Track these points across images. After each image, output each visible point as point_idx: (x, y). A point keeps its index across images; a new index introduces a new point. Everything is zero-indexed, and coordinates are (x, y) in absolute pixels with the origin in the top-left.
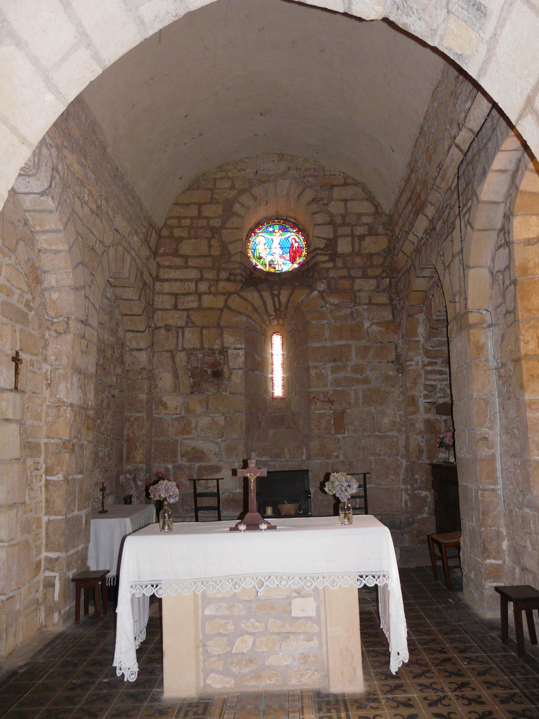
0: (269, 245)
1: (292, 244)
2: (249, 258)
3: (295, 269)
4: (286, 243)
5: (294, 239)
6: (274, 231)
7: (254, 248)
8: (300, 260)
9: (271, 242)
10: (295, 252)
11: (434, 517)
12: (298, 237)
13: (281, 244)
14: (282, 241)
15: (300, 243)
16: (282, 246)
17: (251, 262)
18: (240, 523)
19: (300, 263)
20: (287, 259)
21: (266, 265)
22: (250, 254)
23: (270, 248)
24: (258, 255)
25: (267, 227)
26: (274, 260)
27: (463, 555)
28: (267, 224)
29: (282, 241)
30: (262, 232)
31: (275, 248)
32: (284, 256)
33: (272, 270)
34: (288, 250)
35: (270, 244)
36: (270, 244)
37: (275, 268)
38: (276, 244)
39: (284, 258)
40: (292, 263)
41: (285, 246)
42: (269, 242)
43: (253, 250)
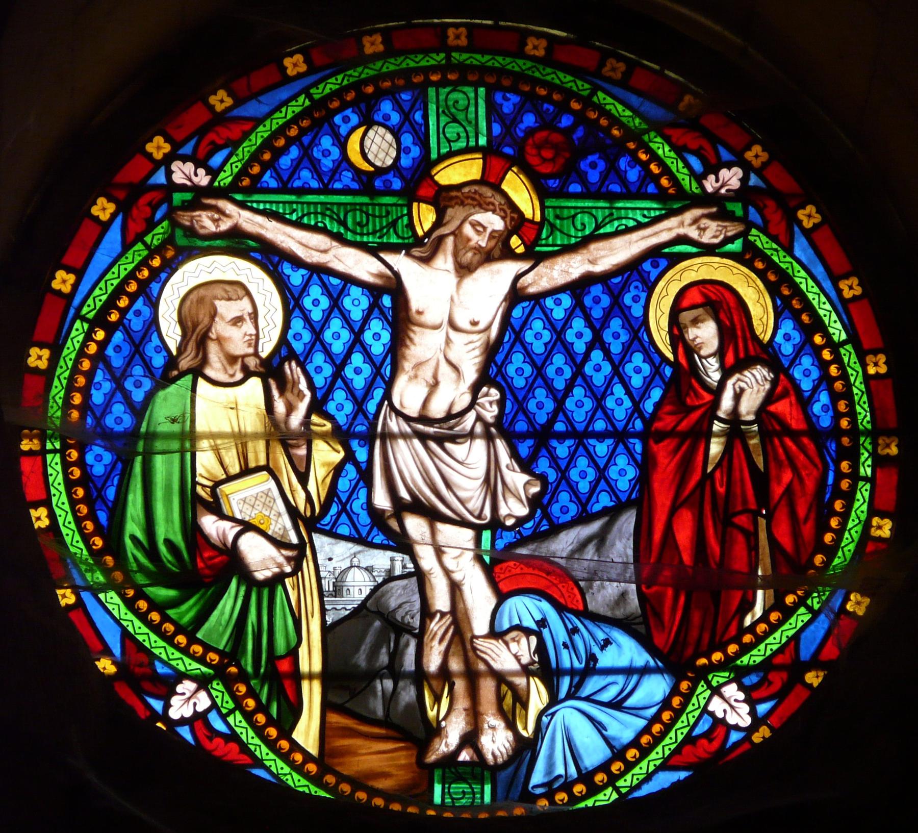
0: (337, 369)
1: (682, 376)
2: (42, 559)
3: (712, 761)
4: (598, 368)
5: (718, 301)
6: (415, 180)
7: (118, 417)
8: (779, 627)
9: (378, 337)
10: (721, 504)
11: (768, 386)
12: (779, 286)
13: (517, 368)
14: (537, 335)
15: (805, 374)
16: (541, 405)
17: (74, 637)
18: (201, 557)
19: (788, 664)
20: (603, 596)
21: (283, 679)
22: (58, 511)
23: (361, 434)
24: (169, 527)
25: (319, 118)
26: (402, 597)
27: (726, 266)
28: (318, 70)
29: (537, 335)
30: (244, 188)
31: (438, 431)
32: (563, 544)
33: (377, 758)
34: (623, 473)
35: (358, 371)
36: (358, 371)
37: (420, 733)
38: (441, 369)
39: (563, 590)
40: (682, 663)
41: (579, 405)
42: (337, 336)
43: (99, 459)
